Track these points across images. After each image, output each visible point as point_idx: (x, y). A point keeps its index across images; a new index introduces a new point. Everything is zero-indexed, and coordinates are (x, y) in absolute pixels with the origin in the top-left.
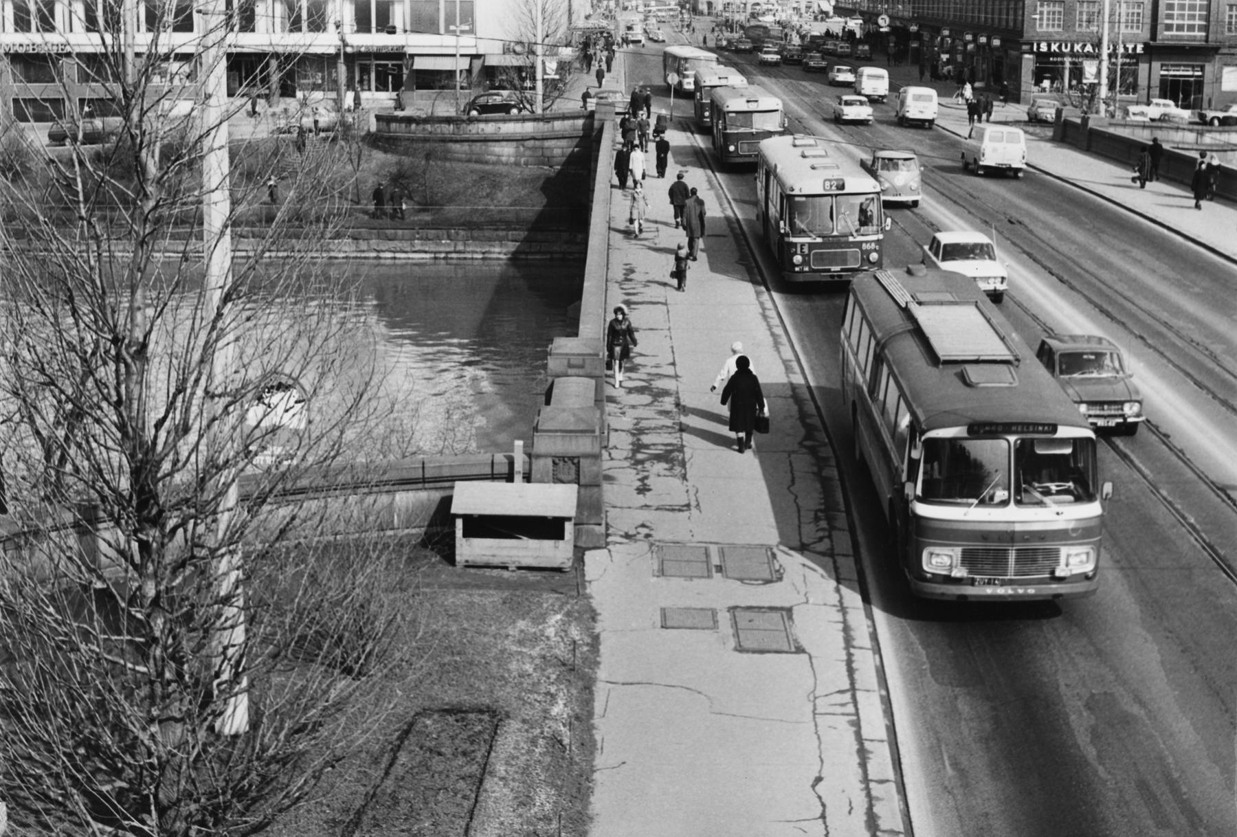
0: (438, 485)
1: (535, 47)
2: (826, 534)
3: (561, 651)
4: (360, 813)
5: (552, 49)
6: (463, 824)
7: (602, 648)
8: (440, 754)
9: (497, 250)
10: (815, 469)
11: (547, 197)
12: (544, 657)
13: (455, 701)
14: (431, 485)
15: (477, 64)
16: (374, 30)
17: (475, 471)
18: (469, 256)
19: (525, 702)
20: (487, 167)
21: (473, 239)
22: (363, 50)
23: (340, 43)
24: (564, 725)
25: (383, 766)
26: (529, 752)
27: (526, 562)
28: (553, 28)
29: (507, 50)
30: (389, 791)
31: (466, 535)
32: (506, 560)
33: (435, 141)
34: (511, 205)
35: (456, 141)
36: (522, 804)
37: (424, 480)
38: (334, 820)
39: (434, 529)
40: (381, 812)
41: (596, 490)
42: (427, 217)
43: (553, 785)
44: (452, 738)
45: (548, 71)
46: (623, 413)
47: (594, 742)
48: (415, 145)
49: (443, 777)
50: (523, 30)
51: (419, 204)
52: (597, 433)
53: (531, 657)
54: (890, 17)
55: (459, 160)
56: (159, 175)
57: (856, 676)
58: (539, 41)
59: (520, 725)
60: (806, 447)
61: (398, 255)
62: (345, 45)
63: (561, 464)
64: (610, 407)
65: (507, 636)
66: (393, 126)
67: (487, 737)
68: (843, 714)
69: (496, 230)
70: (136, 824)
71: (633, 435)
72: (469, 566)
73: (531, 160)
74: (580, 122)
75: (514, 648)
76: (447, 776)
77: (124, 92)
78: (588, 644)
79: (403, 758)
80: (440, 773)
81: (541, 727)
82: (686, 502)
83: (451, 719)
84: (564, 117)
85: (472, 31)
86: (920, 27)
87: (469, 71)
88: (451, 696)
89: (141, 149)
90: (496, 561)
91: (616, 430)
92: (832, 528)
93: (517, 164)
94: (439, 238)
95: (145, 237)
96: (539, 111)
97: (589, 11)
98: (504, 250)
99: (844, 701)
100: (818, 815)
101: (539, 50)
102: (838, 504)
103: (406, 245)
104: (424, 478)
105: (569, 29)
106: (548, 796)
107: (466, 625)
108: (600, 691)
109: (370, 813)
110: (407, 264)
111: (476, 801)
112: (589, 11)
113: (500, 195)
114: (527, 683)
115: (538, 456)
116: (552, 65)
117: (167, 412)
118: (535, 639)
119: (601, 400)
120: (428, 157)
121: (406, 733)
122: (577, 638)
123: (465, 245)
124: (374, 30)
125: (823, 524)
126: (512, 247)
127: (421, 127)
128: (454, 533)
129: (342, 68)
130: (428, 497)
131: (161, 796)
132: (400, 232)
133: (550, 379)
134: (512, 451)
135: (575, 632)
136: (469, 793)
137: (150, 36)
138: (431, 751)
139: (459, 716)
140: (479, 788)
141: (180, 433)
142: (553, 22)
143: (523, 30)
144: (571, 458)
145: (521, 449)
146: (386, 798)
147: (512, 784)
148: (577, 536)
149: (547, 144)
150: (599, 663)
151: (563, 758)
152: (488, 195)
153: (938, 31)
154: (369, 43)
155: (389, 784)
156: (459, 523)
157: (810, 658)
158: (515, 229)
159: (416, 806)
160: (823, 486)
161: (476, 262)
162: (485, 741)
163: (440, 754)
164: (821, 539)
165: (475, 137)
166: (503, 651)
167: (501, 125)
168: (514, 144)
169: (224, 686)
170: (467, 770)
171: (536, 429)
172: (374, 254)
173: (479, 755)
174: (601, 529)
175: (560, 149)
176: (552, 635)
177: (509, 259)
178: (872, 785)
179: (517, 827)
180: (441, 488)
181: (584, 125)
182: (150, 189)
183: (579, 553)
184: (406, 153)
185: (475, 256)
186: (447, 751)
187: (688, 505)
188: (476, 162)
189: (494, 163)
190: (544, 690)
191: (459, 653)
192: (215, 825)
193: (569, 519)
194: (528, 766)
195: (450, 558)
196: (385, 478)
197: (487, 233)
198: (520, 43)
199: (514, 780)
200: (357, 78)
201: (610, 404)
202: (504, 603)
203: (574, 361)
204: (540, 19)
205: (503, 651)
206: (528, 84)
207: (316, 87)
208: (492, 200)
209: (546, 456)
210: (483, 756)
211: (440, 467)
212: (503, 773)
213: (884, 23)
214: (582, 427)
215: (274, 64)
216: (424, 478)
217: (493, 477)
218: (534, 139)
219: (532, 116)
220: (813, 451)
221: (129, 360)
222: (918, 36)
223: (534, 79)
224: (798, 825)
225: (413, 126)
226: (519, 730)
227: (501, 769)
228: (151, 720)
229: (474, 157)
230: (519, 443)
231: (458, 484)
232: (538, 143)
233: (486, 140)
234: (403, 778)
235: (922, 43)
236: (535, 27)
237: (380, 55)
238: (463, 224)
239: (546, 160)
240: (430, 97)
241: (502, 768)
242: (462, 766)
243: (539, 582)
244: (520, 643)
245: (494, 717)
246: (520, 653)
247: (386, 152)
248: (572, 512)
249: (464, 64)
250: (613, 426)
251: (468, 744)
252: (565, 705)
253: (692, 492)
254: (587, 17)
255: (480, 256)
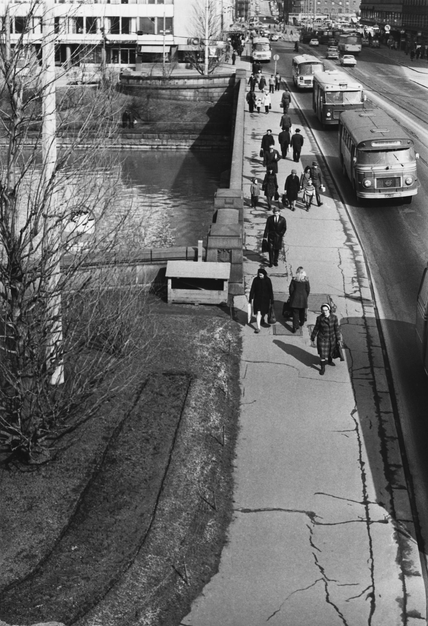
0: (159, 262)
1: (204, 41)
2: (358, 289)
3: (223, 345)
4: (122, 424)
5: (213, 43)
6: (174, 430)
7: (243, 344)
8: (162, 395)
9: (184, 144)
10: (352, 257)
11: (210, 117)
12: (214, 348)
13: (169, 369)
14: (155, 262)
15: (174, 50)
16: (120, 32)
17: (178, 256)
18: (169, 147)
19: (204, 371)
20: (179, 102)
21: (171, 138)
22: (115, 42)
23: (103, 39)
24: (225, 382)
25: (133, 401)
26: (207, 395)
27: (203, 301)
28: (214, 31)
29: (189, 43)
30: (136, 413)
31: (173, 287)
32: (194, 300)
33: (153, 89)
34: (191, 121)
35: (163, 89)
36: (204, 420)
37: (152, 260)
38: (109, 427)
39: (158, 284)
40: (132, 423)
41: (240, 266)
42: (148, 127)
43: (219, 411)
44: (168, 388)
45: (211, 53)
46: (253, 227)
47: (240, 390)
48: (142, 91)
49: (163, 406)
50: (198, 32)
51: (143, 120)
52: (241, 237)
53: (208, 349)
54: (391, 26)
55: (165, 99)
56: (23, 106)
57: (374, 360)
58: (207, 38)
59: (202, 382)
60: (347, 246)
61: (133, 146)
62: (106, 40)
63: (222, 252)
64: (246, 224)
65: (195, 337)
66: (131, 81)
67: (185, 387)
68: (367, 379)
69: (184, 134)
70: (11, 428)
71: (257, 238)
72: (174, 303)
73: (202, 98)
74: (228, 79)
75: (199, 344)
76: (166, 406)
77: (5, 65)
78: (236, 342)
79: (143, 397)
80: (162, 404)
81: (213, 383)
82: (286, 272)
83: (167, 378)
84: (219, 77)
85: (172, 33)
86: (406, 31)
87: (170, 53)
88: (168, 367)
89: (14, 93)
90: (188, 301)
91: (249, 236)
92: (361, 286)
93: (195, 100)
94: (154, 138)
95: (15, 137)
96: (206, 74)
97: (232, 23)
98: (188, 144)
99: (367, 372)
100: (354, 428)
101: (207, 42)
102: (364, 274)
103: (137, 142)
104: (151, 259)
105: (221, 32)
106: (217, 416)
107: (173, 332)
108: (243, 365)
109: (127, 424)
110: (137, 151)
111: (181, 419)
112: (232, 23)
113: (185, 116)
114: (205, 360)
115: (211, 248)
116: (213, 51)
117: (27, 224)
118: (208, 340)
119: (242, 220)
120: (148, 97)
121: (144, 385)
122: (231, 339)
123: (167, 141)
124: (120, 32)
125: (356, 284)
126: (191, 142)
127: (145, 81)
128: (167, 287)
129: (104, 51)
130: (154, 268)
131: (22, 414)
132: (134, 135)
133: (215, 209)
134: (197, 246)
135: (229, 336)
136: (176, 414)
137: (19, 35)
138: (157, 394)
139: (171, 376)
140: (182, 412)
141: (33, 235)
142: (214, 28)
143: (198, 32)
144: (227, 250)
145: (201, 245)
146: (135, 416)
147: (198, 410)
148: (230, 288)
149: (210, 90)
150: (242, 352)
151: (224, 398)
152: (179, 116)
153: (416, 33)
154: (118, 39)
155: (136, 410)
156: (170, 281)
157: (350, 351)
158: (193, 134)
159: (150, 421)
160: (356, 265)
161: (173, 150)
162: (184, 389)
163: (162, 395)
164: (355, 292)
165: (173, 87)
166: (193, 345)
167: (186, 80)
168: (193, 90)
169: (53, 361)
170: (175, 403)
171: (209, 235)
172: (121, 146)
173: (181, 396)
174: (243, 285)
175: (217, 93)
176: (218, 337)
177: (190, 149)
178: (382, 414)
179: (201, 431)
180: (160, 264)
181: (230, 81)
182: (18, 113)
183: (231, 297)
184: (137, 95)
185: (173, 147)
186: (165, 394)
187: (287, 274)
188: (173, 99)
189: (182, 100)
190: (214, 365)
191: (170, 346)
192: (49, 428)
193: (226, 280)
194: (207, 402)
195: (165, 298)
196: (138, 258)
197: (179, 136)
198: (197, 39)
199: (199, 408)
200: (111, 57)
201: (246, 223)
202: (193, 321)
203: (228, 200)
204: (207, 26)
205: (193, 345)
206: (200, 60)
207: (89, 62)
208: (182, 119)
209: (214, 248)
210: (183, 397)
211: (160, 253)
212: (194, 405)
213: (388, 29)
214: (234, 234)
215: (68, 50)
216: (151, 259)
217: (187, 259)
218: (204, 88)
219: (203, 76)
220: (351, 248)
221: (7, 199)
222: (404, 36)
223: (204, 57)
224: (344, 433)
225: (141, 81)
226: (202, 384)
227: (193, 403)
228: (18, 377)
229: (172, 97)
230: (201, 242)
231: (169, 262)
232: (205, 90)
233: (179, 88)
234: (143, 406)
235: (407, 39)
236: (204, 30)
237: (124, 45)
238: (166, 131)
239: (211, 99)
240: (149, 67)
241: (193, 403)
242: (173, 402)
243: (211, 311)
244: (201, 341)
245: (188, 377)
246: (201, 346)
247: (126, 94)
248: (228, 277)
249: (167, 49)
250: (248, 234)
251: (176, 390)
252: (225, 372)
253: (288, 268)
254: (231, 26)
255: (175, 147)
